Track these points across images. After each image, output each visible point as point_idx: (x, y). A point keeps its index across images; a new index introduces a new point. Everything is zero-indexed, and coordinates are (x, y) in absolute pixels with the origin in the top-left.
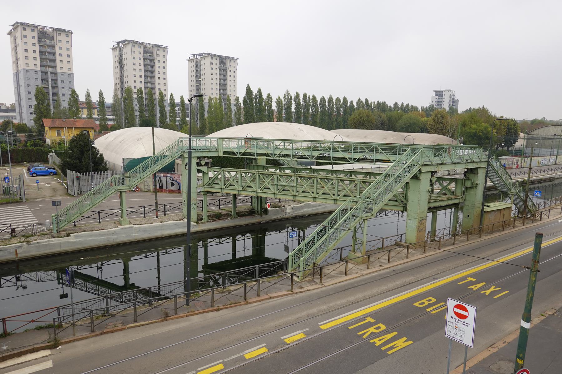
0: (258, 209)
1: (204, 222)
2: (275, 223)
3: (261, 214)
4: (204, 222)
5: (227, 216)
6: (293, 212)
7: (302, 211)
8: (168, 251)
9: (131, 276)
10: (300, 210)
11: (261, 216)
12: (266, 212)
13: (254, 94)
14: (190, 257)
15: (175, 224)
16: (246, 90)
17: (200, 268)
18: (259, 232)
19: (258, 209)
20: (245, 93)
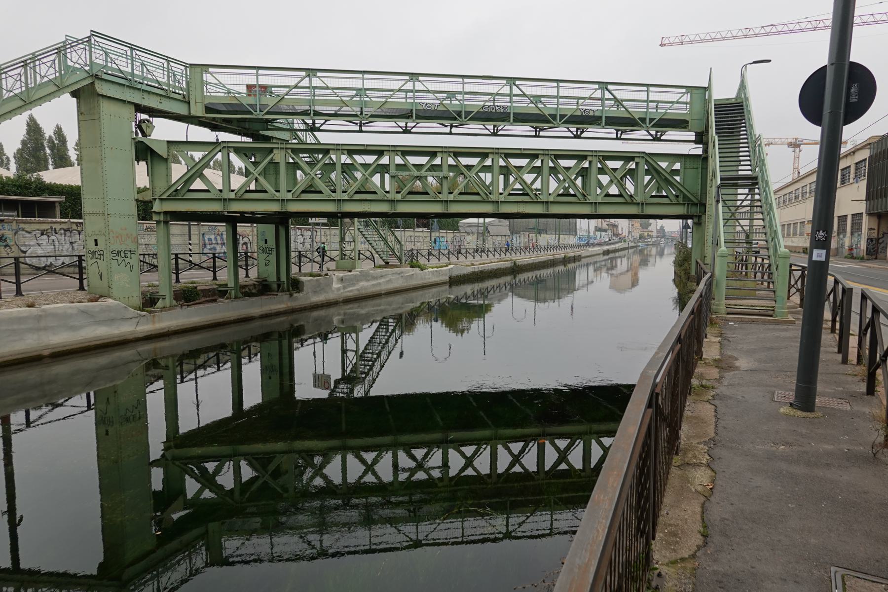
0: (279, 278)
1: (164, 308)
2: (315, 314)
3: (288, 290)
4: (164, 308)
5: (218, 293)
6: (344, 288)
7: (357, 287)
8: (34, 415)
9: (857, 33)
10: (354, 285)
11: (291, 295)
12: (296, 285)
13: (47, 136)
14: (118, 423)
15: (84, 312)
16: (25, 127)
17: (156, 450)
18: (278, 341)
19: (279, 278)
20: (24, 132)
